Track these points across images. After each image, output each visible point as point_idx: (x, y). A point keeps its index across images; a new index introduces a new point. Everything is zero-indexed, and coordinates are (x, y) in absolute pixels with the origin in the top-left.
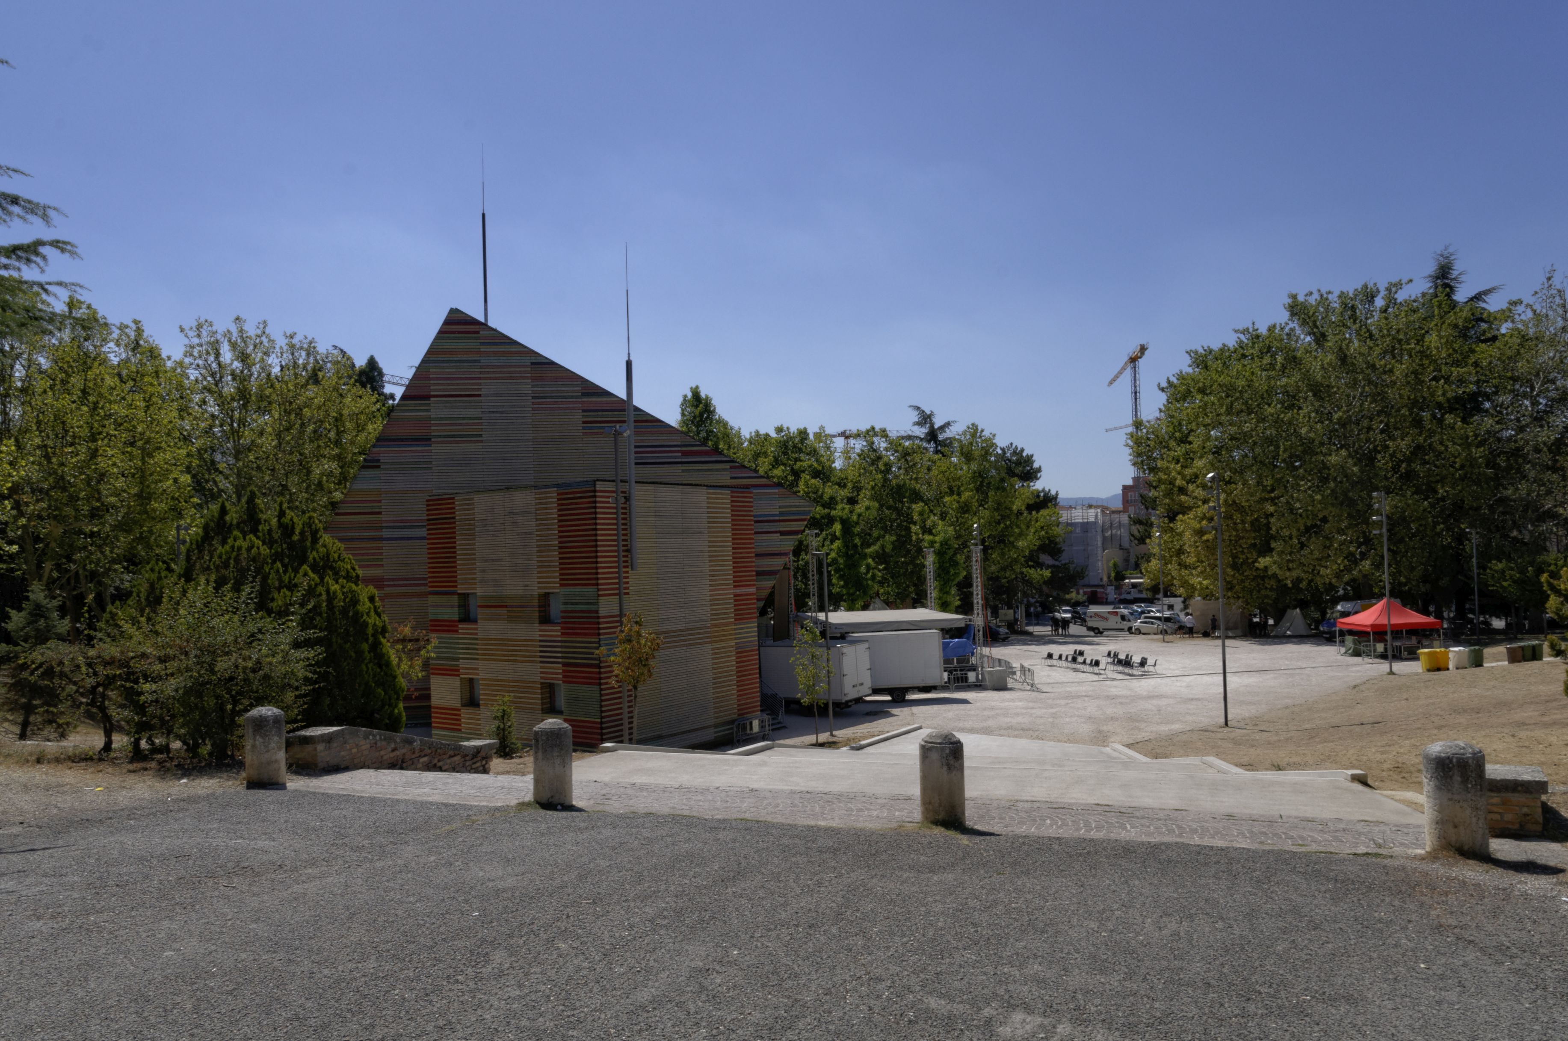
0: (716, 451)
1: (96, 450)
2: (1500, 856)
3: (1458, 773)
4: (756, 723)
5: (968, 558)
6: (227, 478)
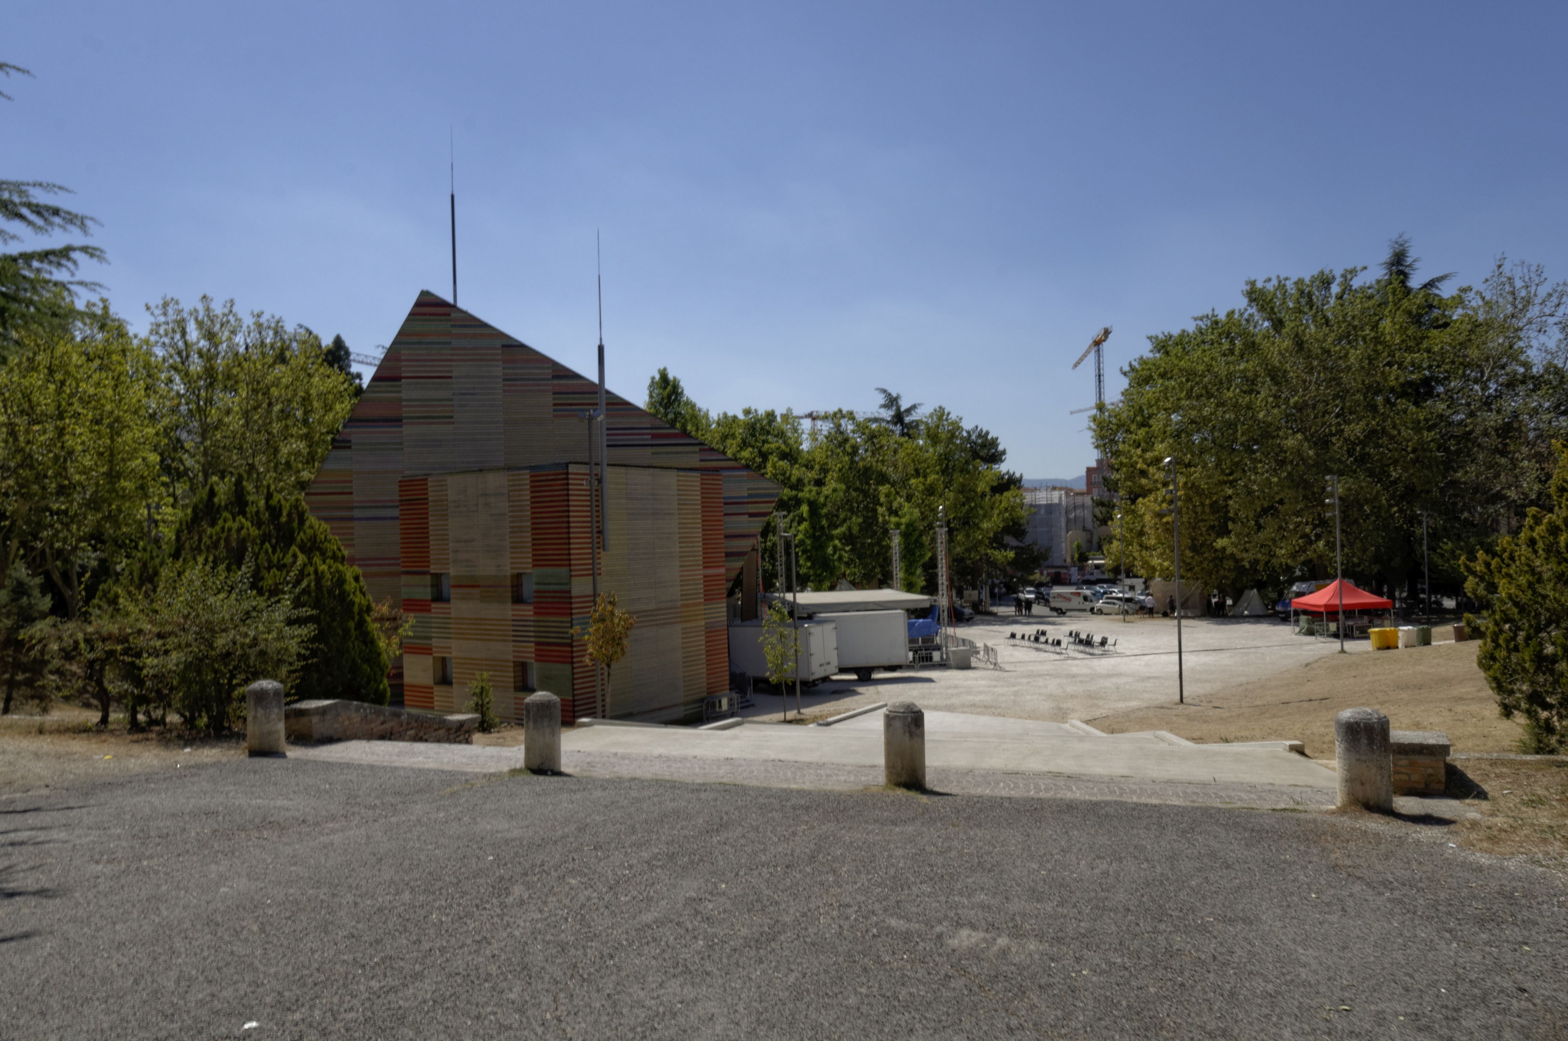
0: (685, 434)
1: (64, 428)
2: (1404, 811)
3: (1366, 737)
4: (725, 702)
5: (933, 540)
6: (193, 456)
